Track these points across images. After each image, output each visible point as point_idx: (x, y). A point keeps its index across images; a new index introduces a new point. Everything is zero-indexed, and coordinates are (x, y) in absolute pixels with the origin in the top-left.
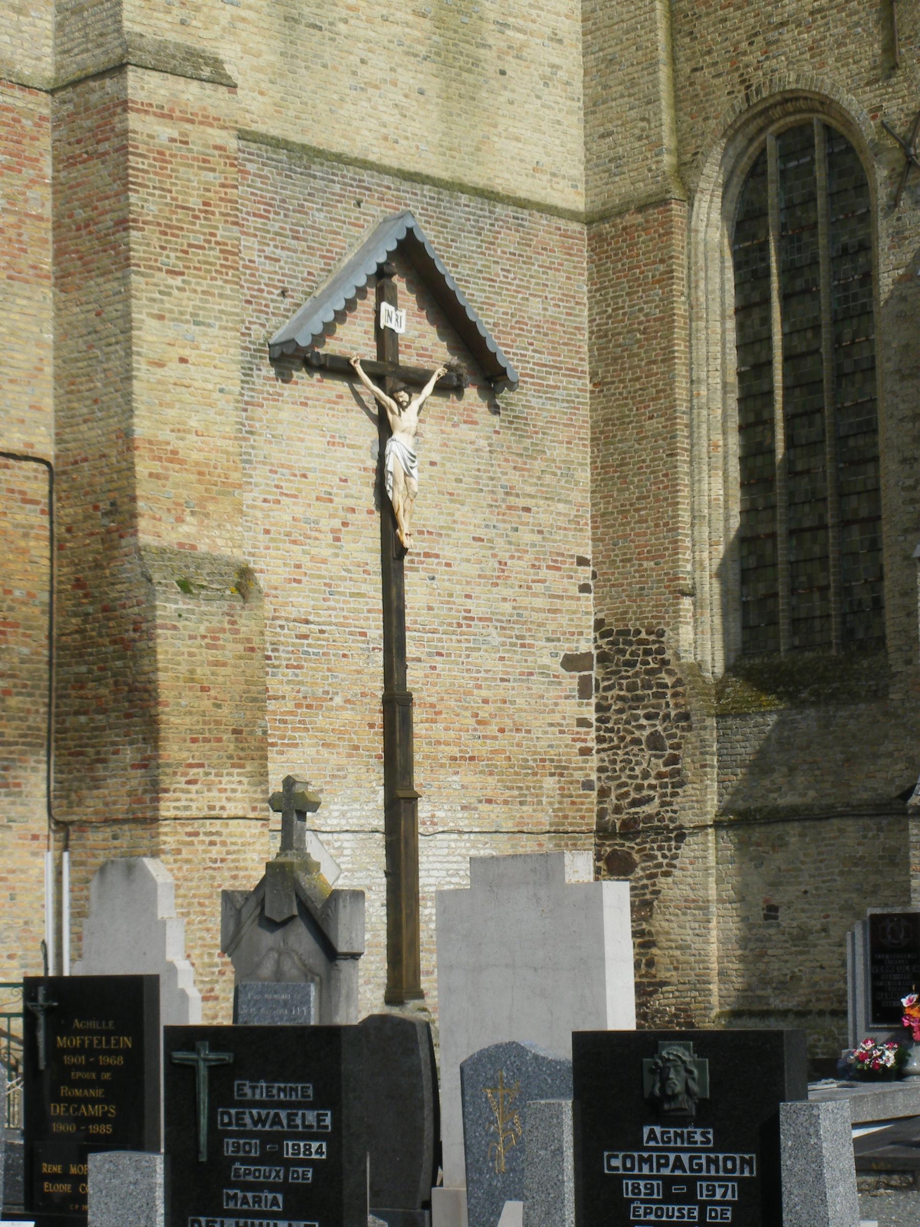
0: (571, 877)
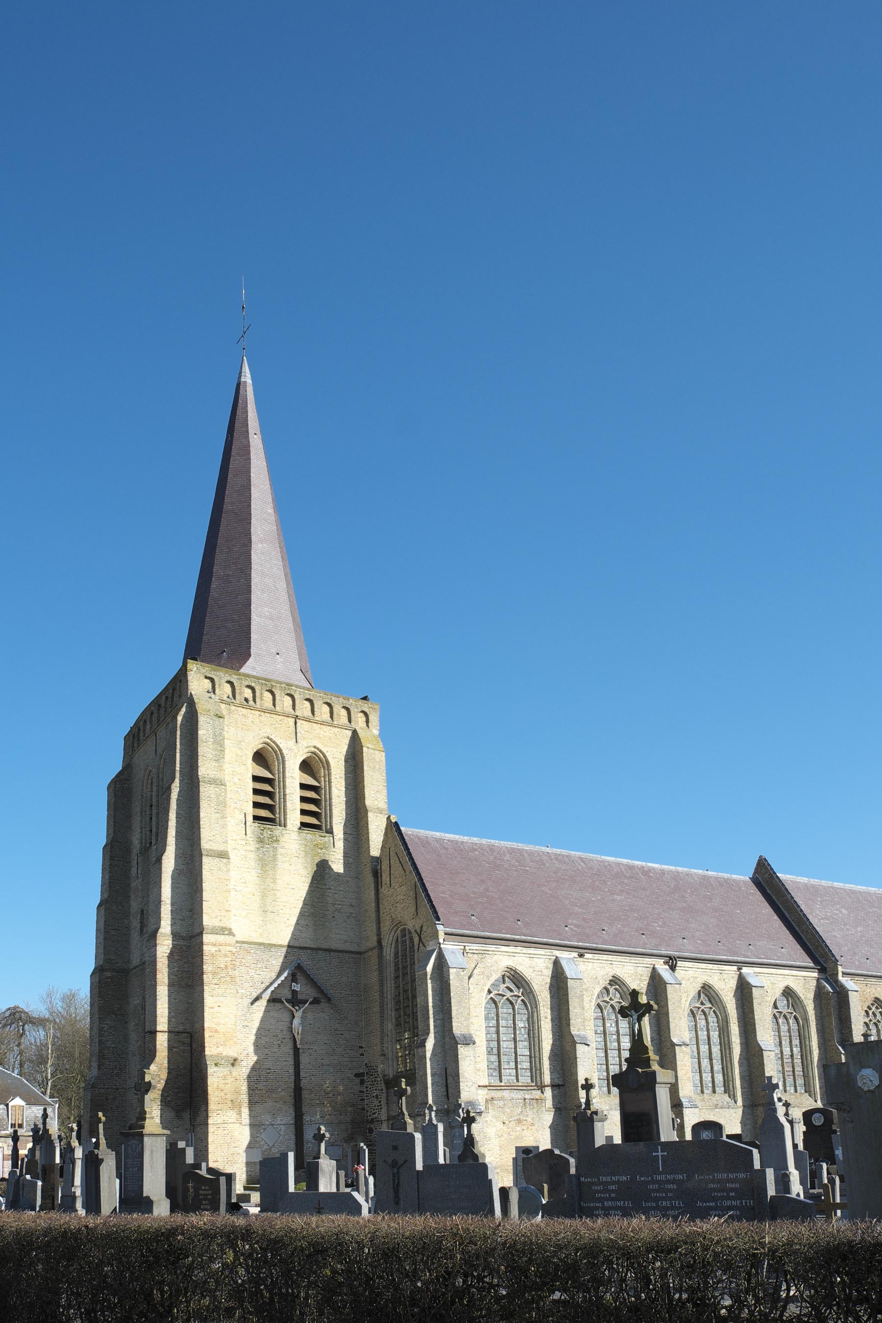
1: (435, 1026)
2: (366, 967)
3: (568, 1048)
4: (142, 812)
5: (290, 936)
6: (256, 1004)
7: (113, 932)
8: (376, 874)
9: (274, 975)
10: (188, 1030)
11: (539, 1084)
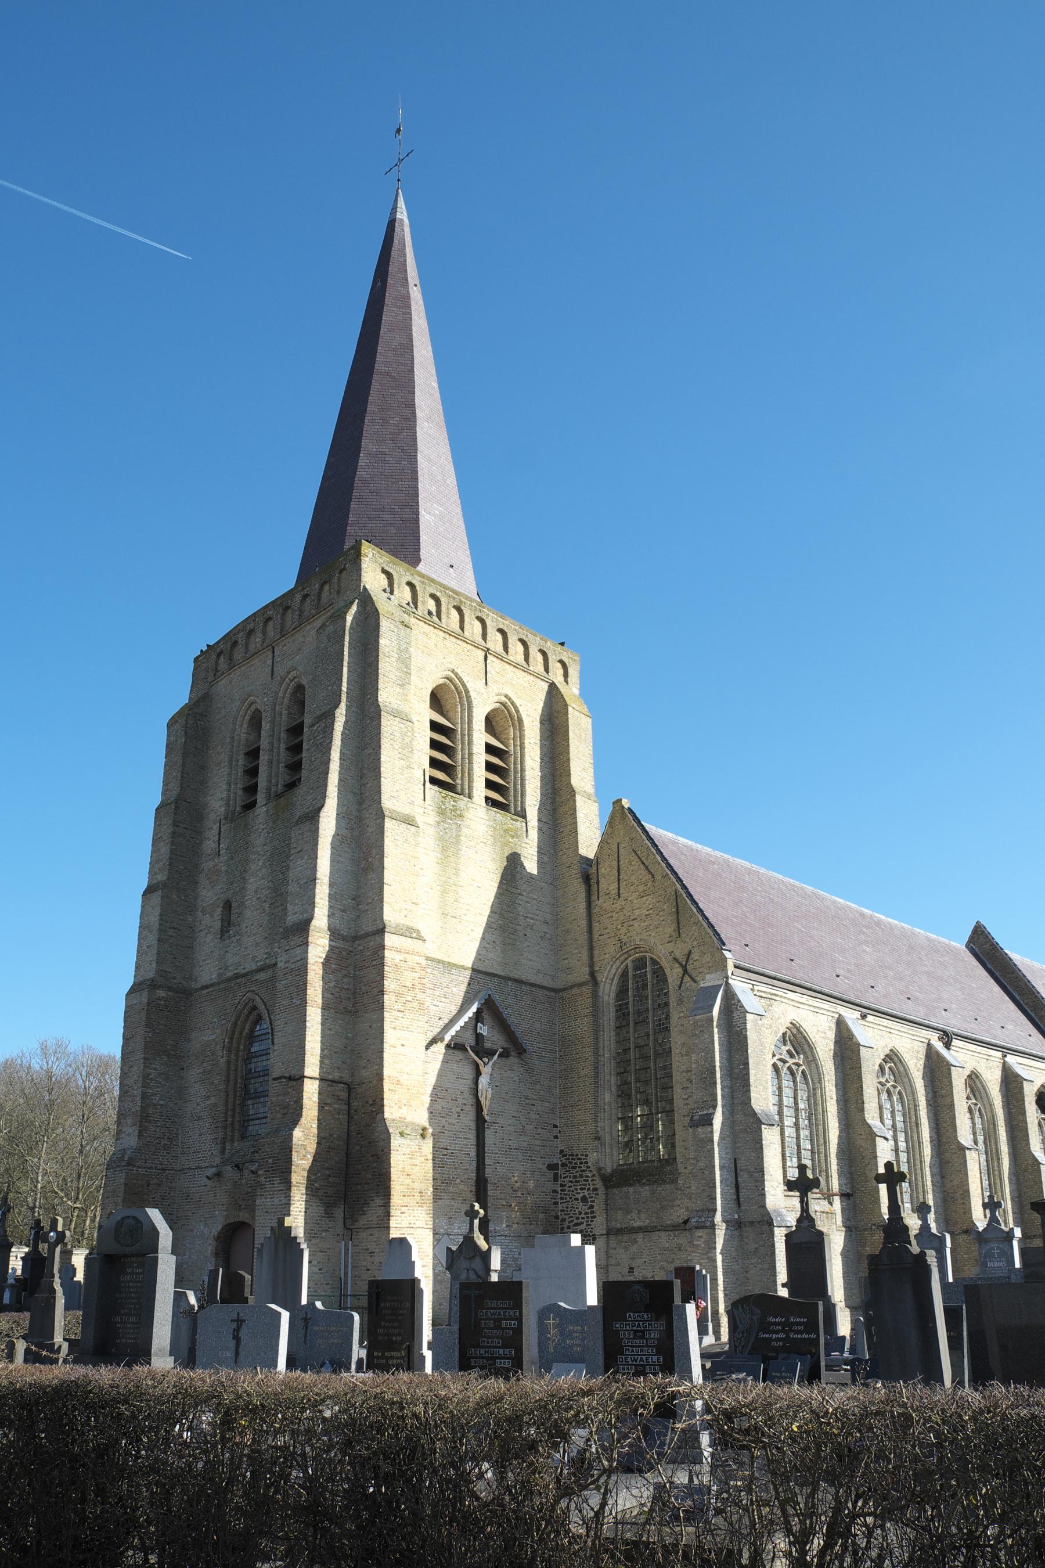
0: (573, 1244)
1: (723, 1096)
2: (608, 1006)
3: (860, 1142)
4: (230, 761)
5: (474, 954)
6: (432, 1048)
7: (171, 932)
8: (587, 879)
9: (454, 1009)
10: (345, 1080)
11: (825, 1191)
